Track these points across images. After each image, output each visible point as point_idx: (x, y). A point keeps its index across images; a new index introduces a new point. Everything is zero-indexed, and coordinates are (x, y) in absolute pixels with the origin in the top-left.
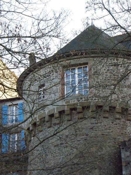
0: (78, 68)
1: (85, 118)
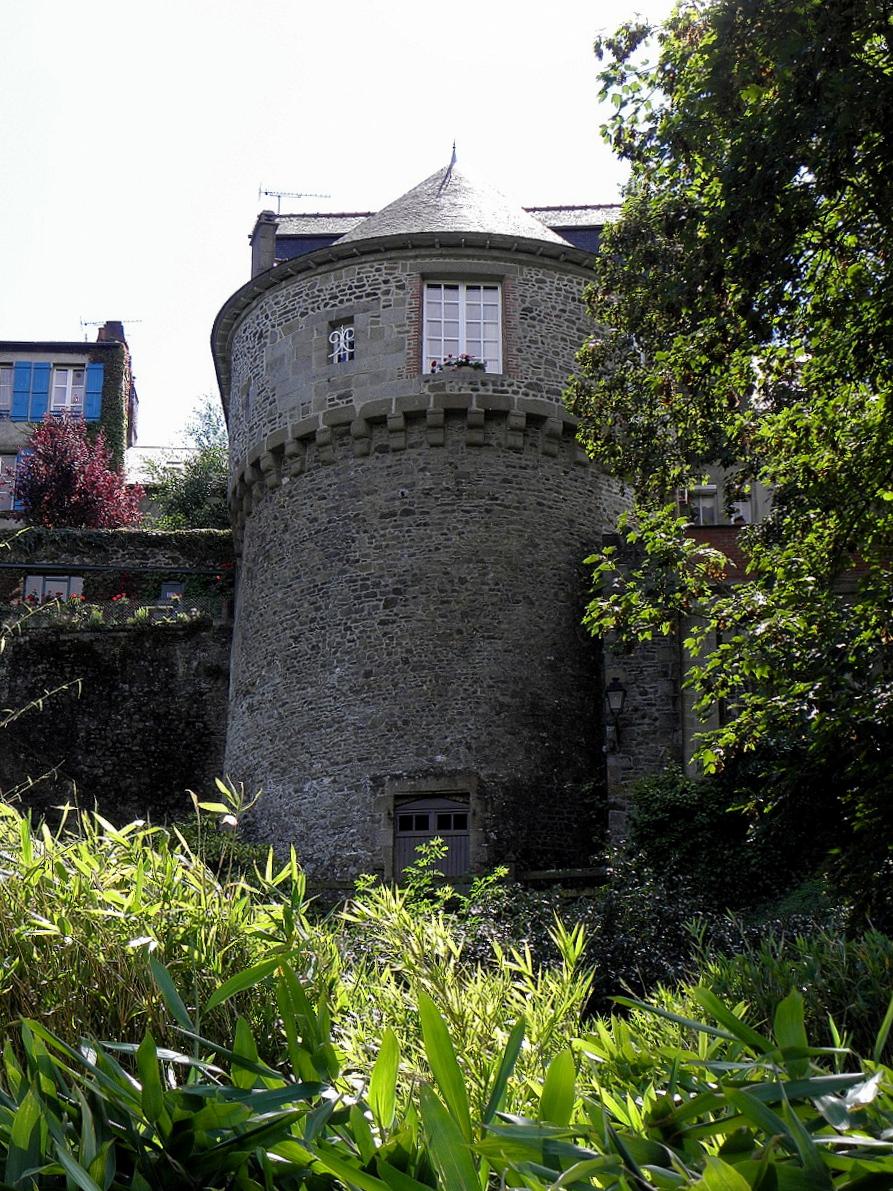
0: (468, 288)
1: (489, 445)
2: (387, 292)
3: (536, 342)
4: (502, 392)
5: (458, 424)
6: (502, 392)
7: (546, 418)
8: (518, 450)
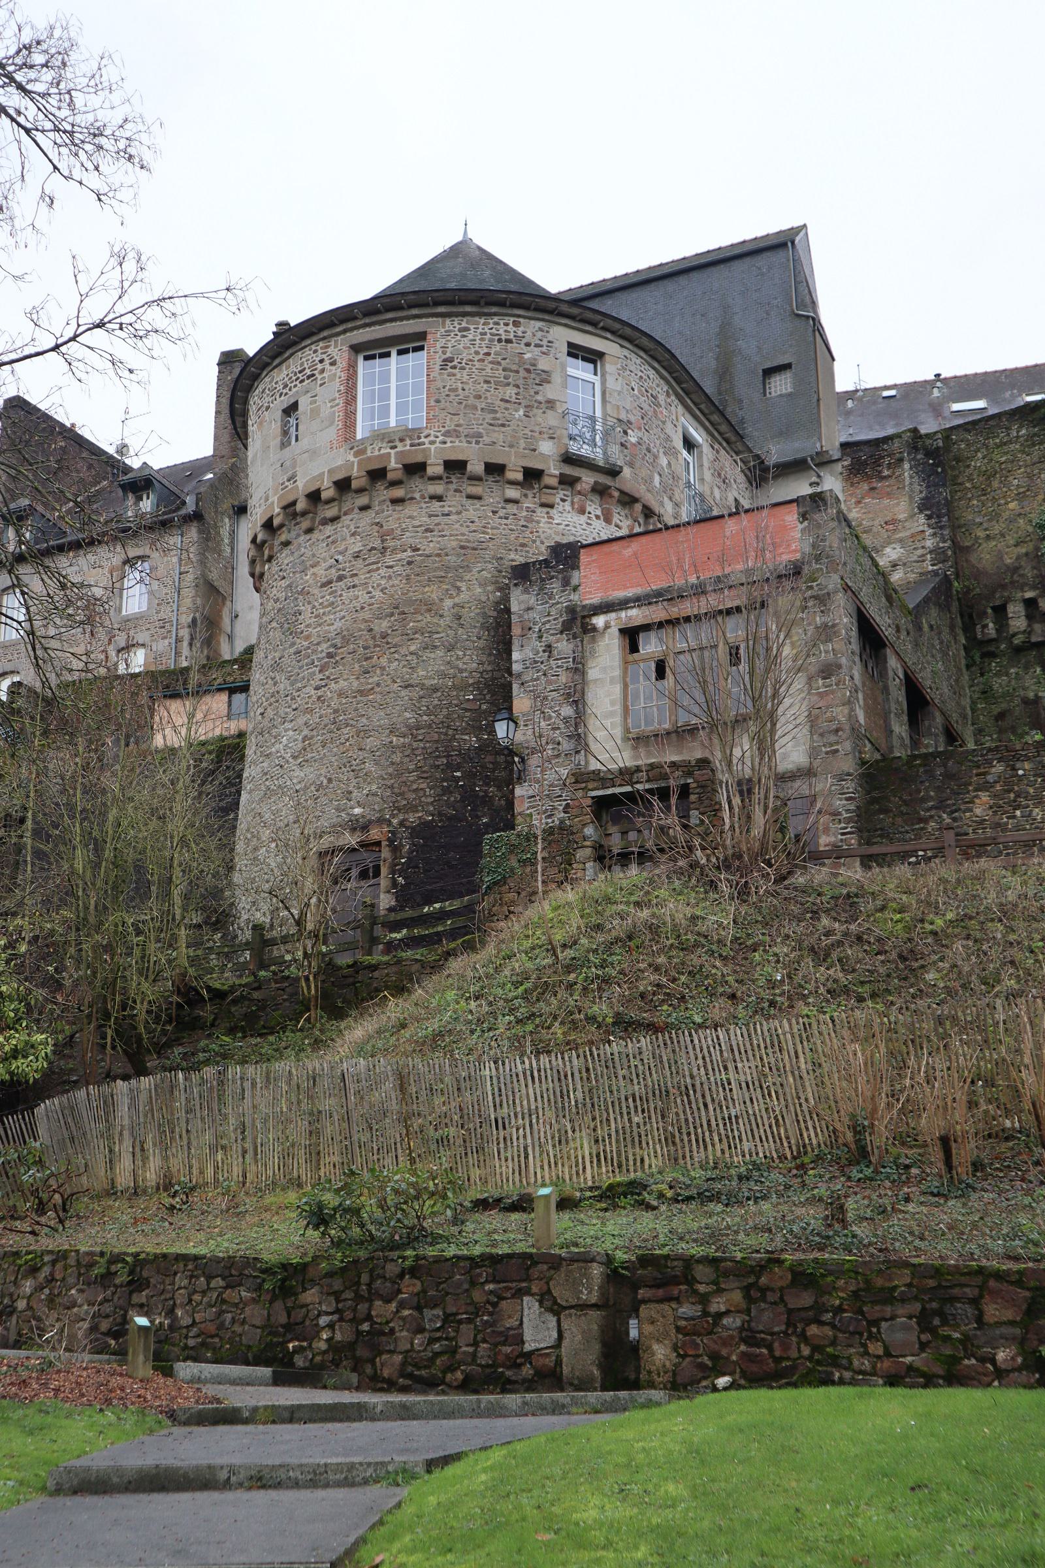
1: (412, 498)
2: (323, 371)
3: (456, 390)
4: (419, 444)
5: (380, 486)
6: (419, 444)
7: (542, 472)
8: (439, 498)
